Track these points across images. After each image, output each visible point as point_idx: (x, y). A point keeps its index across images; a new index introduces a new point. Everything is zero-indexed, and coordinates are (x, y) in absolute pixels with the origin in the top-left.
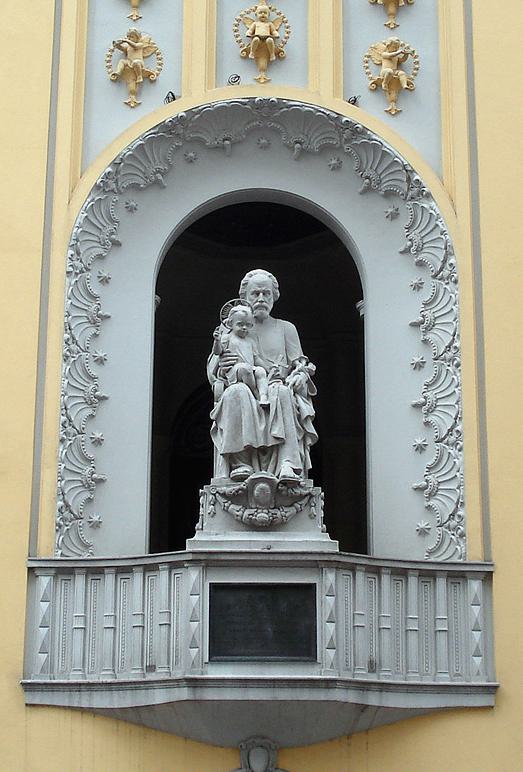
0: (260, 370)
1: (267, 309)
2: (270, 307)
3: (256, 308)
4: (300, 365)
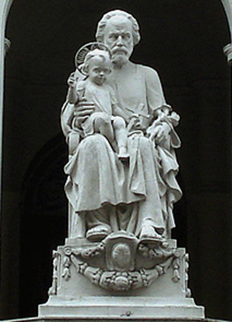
0: (118, 120)
1: (126, 53)
2: (130, 51)
3: (115, 52)
4: (162, 115)
